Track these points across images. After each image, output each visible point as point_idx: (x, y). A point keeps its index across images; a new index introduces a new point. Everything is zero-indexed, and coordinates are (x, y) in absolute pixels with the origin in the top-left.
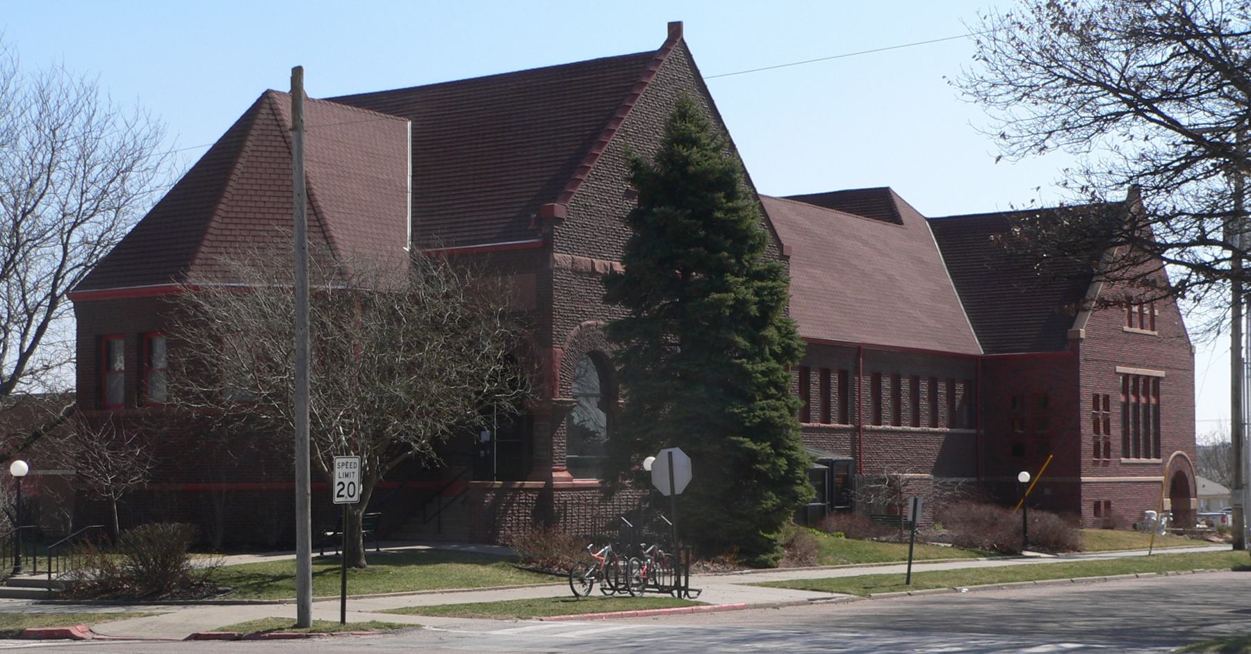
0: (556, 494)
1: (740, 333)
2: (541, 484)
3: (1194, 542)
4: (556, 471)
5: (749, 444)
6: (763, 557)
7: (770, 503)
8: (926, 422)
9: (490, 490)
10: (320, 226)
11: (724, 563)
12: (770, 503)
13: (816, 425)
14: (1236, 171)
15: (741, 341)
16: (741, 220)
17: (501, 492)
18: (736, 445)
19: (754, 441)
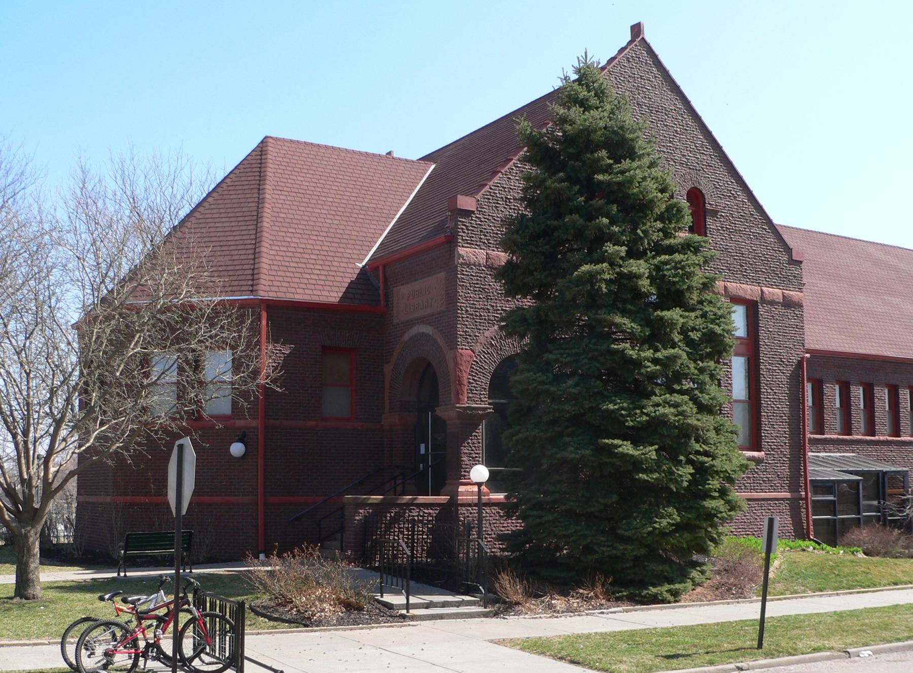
0: (462, 510)
1: (624, 313)
2: (443, 499)
3: (881, 566)
4: (787, 499)
5: (627, 448)
6: (653, 590)
7: (664, 522)
8: (862, 430)
9: (363, 505)
10: (260, 172)
11: (587, 599)
12: (664, 522)
13: (882, 438)
14: (588, 67)
15: (626, 323)
16: (631, 181)
17: (380, 509)
18: (610, 449)
19: (636, 443)
